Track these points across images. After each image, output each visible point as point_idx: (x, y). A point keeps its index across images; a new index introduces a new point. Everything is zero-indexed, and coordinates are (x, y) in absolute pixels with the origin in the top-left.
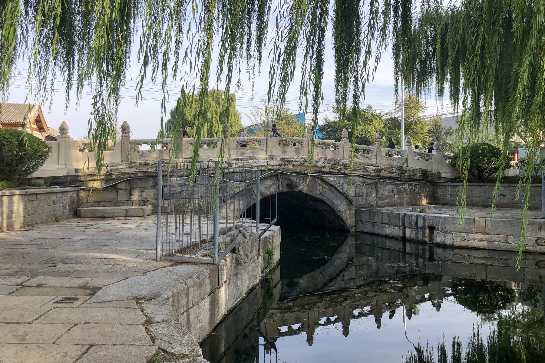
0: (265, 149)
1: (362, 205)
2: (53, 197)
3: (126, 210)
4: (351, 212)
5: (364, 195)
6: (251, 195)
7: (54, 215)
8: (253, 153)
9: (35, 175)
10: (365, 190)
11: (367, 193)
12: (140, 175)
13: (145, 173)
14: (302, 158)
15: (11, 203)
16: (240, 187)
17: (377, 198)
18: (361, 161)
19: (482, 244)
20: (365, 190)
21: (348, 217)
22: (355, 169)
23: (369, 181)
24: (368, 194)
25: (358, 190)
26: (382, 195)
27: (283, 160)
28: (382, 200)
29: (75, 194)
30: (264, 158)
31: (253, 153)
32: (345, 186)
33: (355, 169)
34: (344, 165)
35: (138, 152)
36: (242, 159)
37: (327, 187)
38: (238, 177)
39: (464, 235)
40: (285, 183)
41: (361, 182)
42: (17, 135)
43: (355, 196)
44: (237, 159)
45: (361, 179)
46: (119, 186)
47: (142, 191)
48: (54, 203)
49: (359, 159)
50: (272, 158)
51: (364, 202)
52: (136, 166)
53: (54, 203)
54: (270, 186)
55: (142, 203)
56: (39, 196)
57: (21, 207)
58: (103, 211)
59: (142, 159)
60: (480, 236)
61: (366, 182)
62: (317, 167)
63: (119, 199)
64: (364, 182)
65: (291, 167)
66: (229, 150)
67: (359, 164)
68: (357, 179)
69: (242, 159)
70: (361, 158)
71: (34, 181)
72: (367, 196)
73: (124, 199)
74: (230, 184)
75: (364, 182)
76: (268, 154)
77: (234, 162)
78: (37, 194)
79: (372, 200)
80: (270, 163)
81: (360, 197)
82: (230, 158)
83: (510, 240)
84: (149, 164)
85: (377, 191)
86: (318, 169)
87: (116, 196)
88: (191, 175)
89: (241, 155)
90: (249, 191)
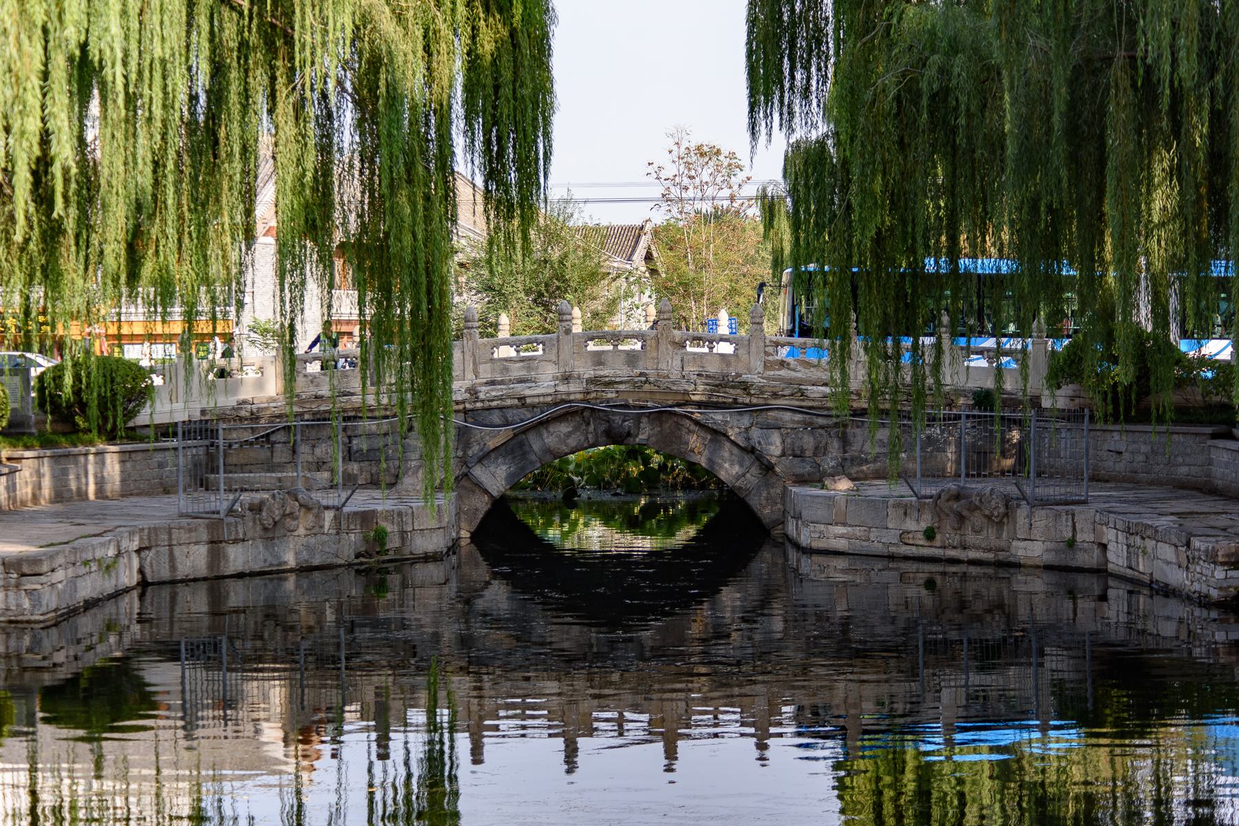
0: (554, 359)
1: (803, 475)
2: (159, 457)
3: (280, 480)
4: (772, 491)
5: (808, 453)
6: (524, 454)
7: (161, 484)
8: (529, 369)
9: (143, 418)
10: (808, 442)
11: (817, 448)
12: (306, 417)
13: (315, 414)
14: (641, 375)
15: (102, 463)
16: (500, 436)
17: (845, 459)
18: (799, 375)
19: (841, 545)
20: (808, 442)
21: (764, 502)
22: (775, 395)
23: (821, 421)
24: (820, 450)
25: (789, 440)
26: (861, 452)
27: (594, 381)
28: (860, 464)
29: (201, 451)
30: (550, 377)
31: (529, 369)
32: (755, 433)
33: (775, 395)
34: (745, 387)
35: (305, 376)
36: (502, 382)
37: (709, 437)
38: (496, 417)
39: (822, 527)
40: (603, 428)
41: (798, 422)
42: (131, 374)
43: (783, 454)
44: (492, 383)
45: (798, 417)
46: (273, 438)
47: (314, 446)
48: (161, 465)
49: (794, 370)
50: (566, 378)
51: (808, 468)
52: (302, 402)
53: (161, 465)
54: (568, 435)
55: (314, 467)
56: (133, 455)
57: (117, 467)
58: (243, 481)
59: (312, 388)
60: (841, 530)
61: (810, 424)
62: (677, 392)
63: (276, 460)
64: (806, 424)
65: (614, 395)
66: (475, 364)
67: (790, 382)
68: (787, 416)
69: (502, 382)
70: (799, 368)
71: (139, 432)
72: (815, 454)
73: (284, 460)
74: (479, 432)
75: (806, 424)
76: (562, 370)
77: (484, 389)
78: (130, 452)
79: (831, 464)
80: (562, 388)
81: (795, 456)
82: (478, 381)
83: (872, 536)
84: (322, 397)
85: (845, 442)
86: (679, 398)
87: (269, 454)
88: (879, 239)
89: (502, 373)
90: (521, 445)
